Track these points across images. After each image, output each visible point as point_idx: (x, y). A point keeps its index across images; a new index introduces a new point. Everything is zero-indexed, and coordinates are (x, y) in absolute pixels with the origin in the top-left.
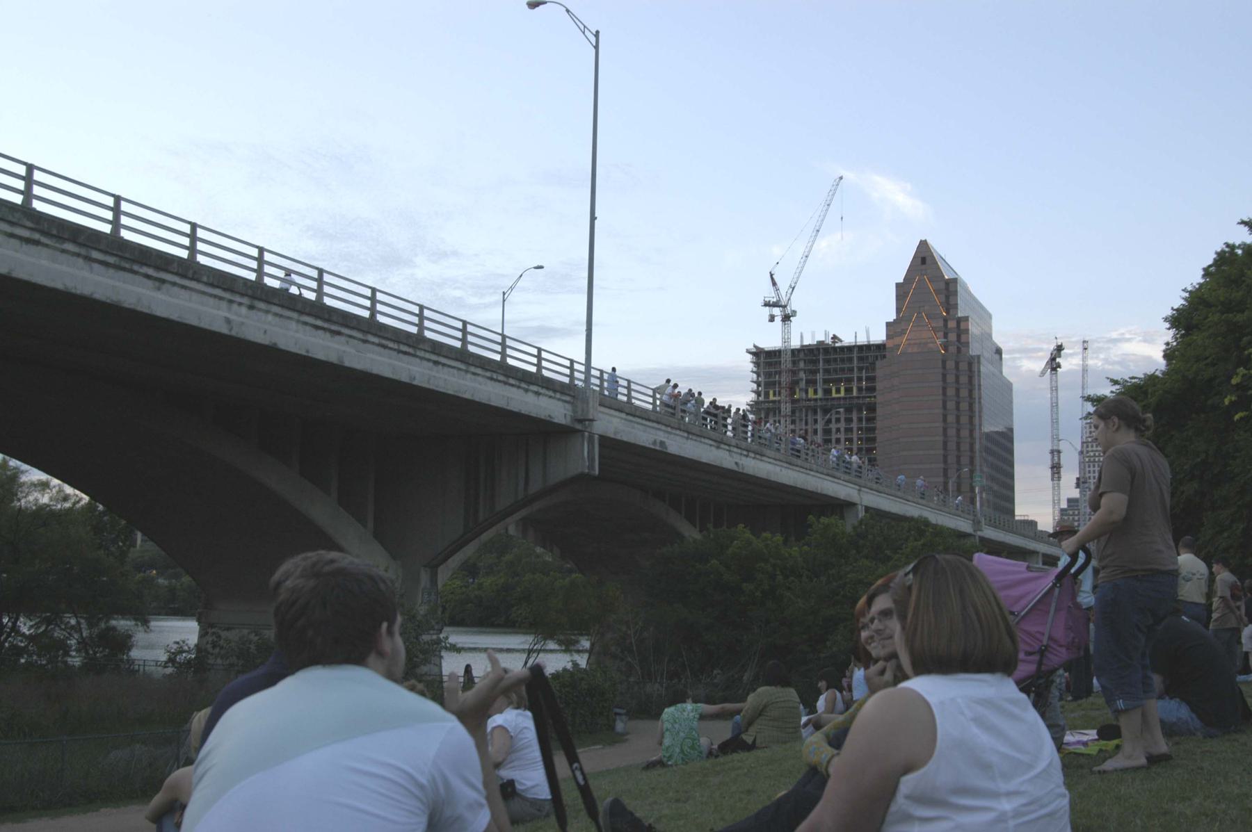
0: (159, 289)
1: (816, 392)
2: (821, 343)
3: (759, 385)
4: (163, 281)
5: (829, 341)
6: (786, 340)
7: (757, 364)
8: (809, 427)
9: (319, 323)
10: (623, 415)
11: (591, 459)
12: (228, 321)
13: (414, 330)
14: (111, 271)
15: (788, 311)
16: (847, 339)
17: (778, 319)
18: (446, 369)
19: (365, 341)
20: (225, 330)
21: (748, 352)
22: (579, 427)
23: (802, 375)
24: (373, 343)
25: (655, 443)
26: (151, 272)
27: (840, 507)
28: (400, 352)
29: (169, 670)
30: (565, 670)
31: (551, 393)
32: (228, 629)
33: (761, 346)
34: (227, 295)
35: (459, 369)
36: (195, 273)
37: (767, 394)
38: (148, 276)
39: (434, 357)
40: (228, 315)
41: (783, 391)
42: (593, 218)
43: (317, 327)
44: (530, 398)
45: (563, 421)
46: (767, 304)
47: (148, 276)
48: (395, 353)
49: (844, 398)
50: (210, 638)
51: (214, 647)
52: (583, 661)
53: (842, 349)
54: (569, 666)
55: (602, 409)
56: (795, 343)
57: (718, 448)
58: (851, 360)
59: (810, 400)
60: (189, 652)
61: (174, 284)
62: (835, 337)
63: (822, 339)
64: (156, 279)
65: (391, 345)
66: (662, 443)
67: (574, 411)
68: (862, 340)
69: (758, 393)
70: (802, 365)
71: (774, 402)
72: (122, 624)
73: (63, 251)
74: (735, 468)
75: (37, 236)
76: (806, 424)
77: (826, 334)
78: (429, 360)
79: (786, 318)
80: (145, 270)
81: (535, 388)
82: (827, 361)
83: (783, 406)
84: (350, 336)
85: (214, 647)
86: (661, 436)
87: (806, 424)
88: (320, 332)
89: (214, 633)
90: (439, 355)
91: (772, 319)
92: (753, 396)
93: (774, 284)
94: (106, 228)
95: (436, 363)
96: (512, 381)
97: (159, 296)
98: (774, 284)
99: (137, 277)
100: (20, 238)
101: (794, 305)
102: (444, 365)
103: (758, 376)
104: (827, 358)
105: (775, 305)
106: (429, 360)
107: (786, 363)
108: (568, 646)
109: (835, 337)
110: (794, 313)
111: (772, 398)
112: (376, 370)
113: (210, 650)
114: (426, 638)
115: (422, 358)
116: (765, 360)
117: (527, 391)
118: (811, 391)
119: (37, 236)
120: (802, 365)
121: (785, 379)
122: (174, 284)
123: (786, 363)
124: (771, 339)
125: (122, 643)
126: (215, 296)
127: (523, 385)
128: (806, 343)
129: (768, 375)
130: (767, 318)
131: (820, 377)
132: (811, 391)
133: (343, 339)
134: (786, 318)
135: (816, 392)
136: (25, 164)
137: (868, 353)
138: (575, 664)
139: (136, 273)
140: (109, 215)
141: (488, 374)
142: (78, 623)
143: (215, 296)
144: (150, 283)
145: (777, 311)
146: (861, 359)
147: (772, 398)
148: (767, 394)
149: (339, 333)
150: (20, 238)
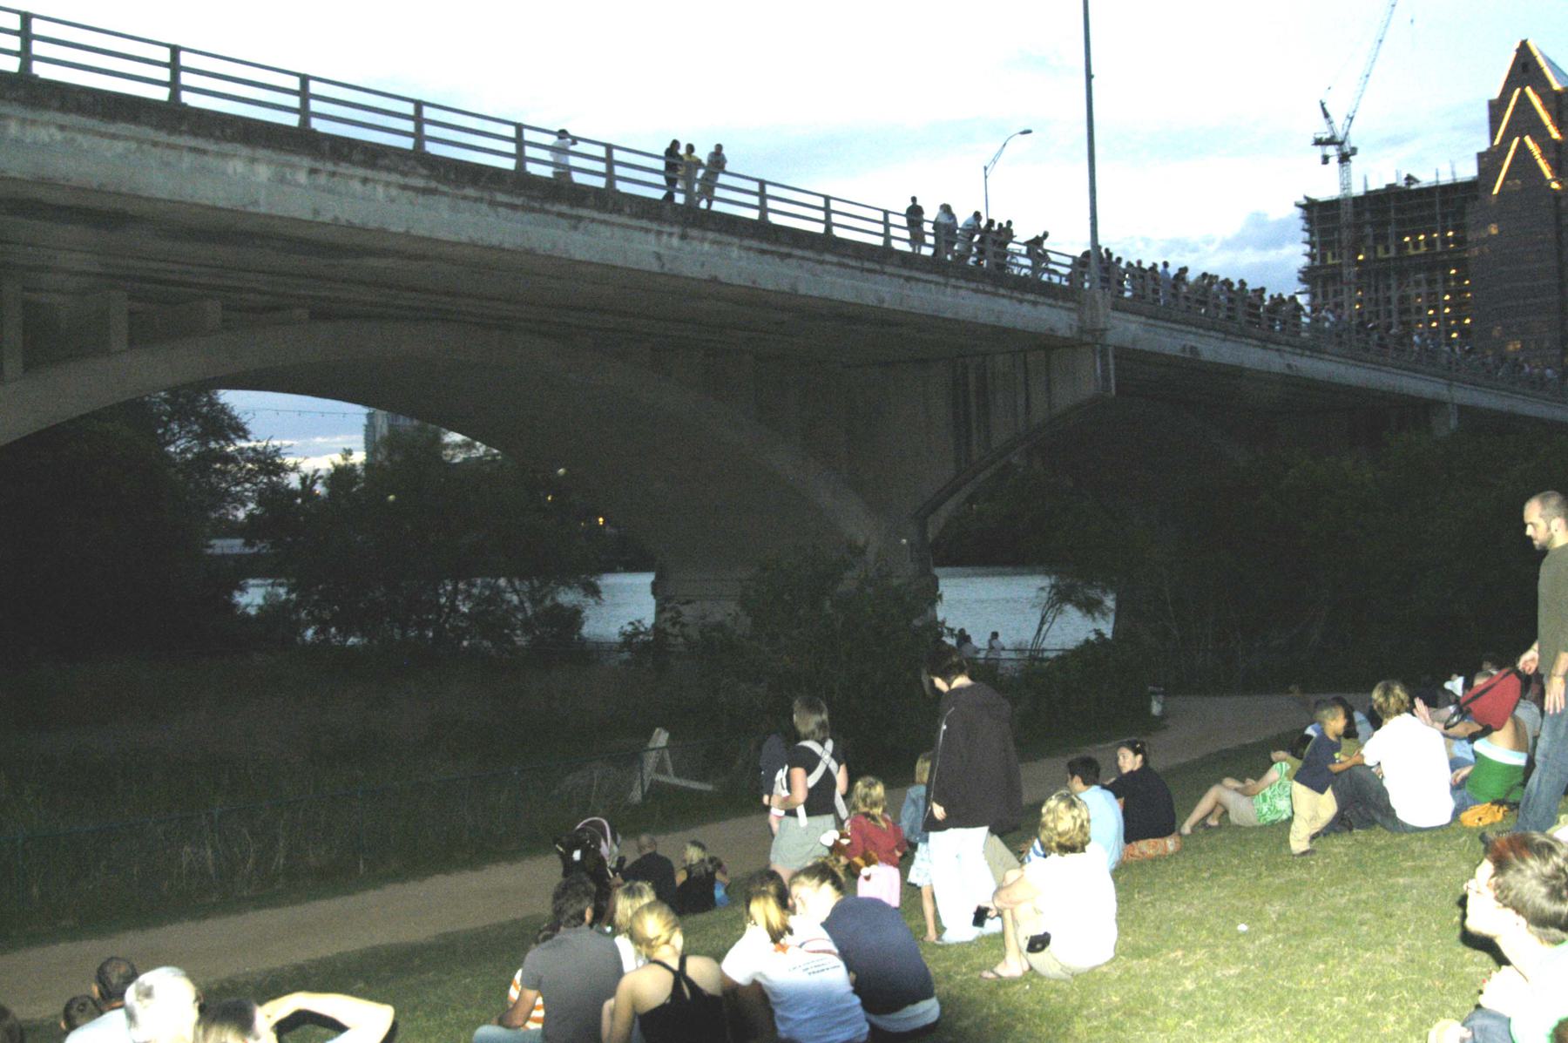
0: (575, 228)
1: (1387, 250)
2: (1390, 187)
3: (1313, 247)
4: (580, 219)
5: (1402, 183)
6: (1346, 186)
7: (1308, 219)
8: (1381, 294)
9: (765, 246)
10: (1143, 319)
11: (1106, 379)
12: (659, 257)
13: (879, 241)
14: (519, 214)
15: (1347, 149)
16: (1426, 179)
17: (1334, 160)
18: (921, 285)
19: (822, 262)
20: (655, 267)
21: (1298, 205)
22: (1087, 338)
23: (1368, 230)
24: (832, 263)
25: (1184, 349)
26: (564, 208)
27: (1425, 409)
28: (863, 270)
29: (626, 656)
30: (1087, 641)
31: (1050, 301)
32: (688, 602)
33: (1313, 196)
34: (655, 226)
35: (937, 284)
36: (615, 204)
37: (1324, 257)
38: (560, 215)
39: (906, 273)
40: (656, 249)
41: (1345, 252)
42: (1089, 77)
43: (763, 252)
44: (1026, 308)
45: (1068, 334)
46: (1318, 142)
47: (560, 215)
48: (858, 273)
49: (1425, 255)
50: (668, 615)
51: (674, 625)
52: (1107, 628)
53: (1421, 191)
54: (1093, 637)
55: (1117, 314)
56: (1357, 190)
57: (1264, 348)
58: (1431, 205)
59: (1382, 260)
60: (646, 633)
61: (593, 220)
62: (1409, 178)
63: (1392, 181)
64: (571, 217)
65: (853, 263)
66: (1193, 349)
67: (1080, 319)
68: (1446, 179)
69: (1311, 256)
70: (1368, 216)
71: (1334, 266)
72: (568, 597)
73: (465, 198)
74: (1287, 371)
75: (433, 184)
76: (1376, 290)
77: (1397, 174)
78: (900, 276)
79: (1344, 158)
80: (558, 208)
81: (1031, 297)
82: (1400, 210)
83: (1345, 271)
84: (803, 258)
85: (674, 625)
86: (1191, 341)
87: (1376, 290)
88: (768, 258)
89: (672, 609)
90: (911, 269)
91: (1326, 160)
92: (1305, 261)
93: (1326, 115)
94: (509, 164)
95: (908, 279)
96: (1002, 291)
97: (577, 236)
98: (1326, 115)
99: (549, 218)
100: (415, 189)
101: (1353, 141)
102: (918, 280)
103: (1312, 235)
104: (1401, 205)
105: (1330, 141)
106: (900, 276)
107: (1346, 215)
108: (1090, 607)
109: (1409, 178)
110: (1354, 151)
111: (1330, 262)
112: (837, 295)
113: (669, 630)
114: (917, 622)
115: (892, 275)
116: (1318, 214)
117: (1021, 301)
118: (1380, 249)
119: (433, 184)
120: (1368, 216)
121: (1346, 236)
122: (593, 220)
123: (1346, 215)
124: (1327, 186)
125: (574, 617)
126: (641, 229)
127: (1016, 294)
128: (1372, 188)
129: (1323, 232)
130: (1320, 160)
131: (1391, 230)
132: (1380, 249)
133: (794, 262)
134: (1344, 158)
135: (1387, 250)
136: (411, 100)
137: (1453, 197)
138: (1099, 633)
139: (547, 212)
140: (511, 148)
141: (973, 285)
142: (522, 602)
143: (641, 229)
144: (565, 223)
145: (1331, 150)
146: (1444, 203)
147: (1330, 262)
148: (1324, 257)
149: (789, 256)
150: (415, 189)
